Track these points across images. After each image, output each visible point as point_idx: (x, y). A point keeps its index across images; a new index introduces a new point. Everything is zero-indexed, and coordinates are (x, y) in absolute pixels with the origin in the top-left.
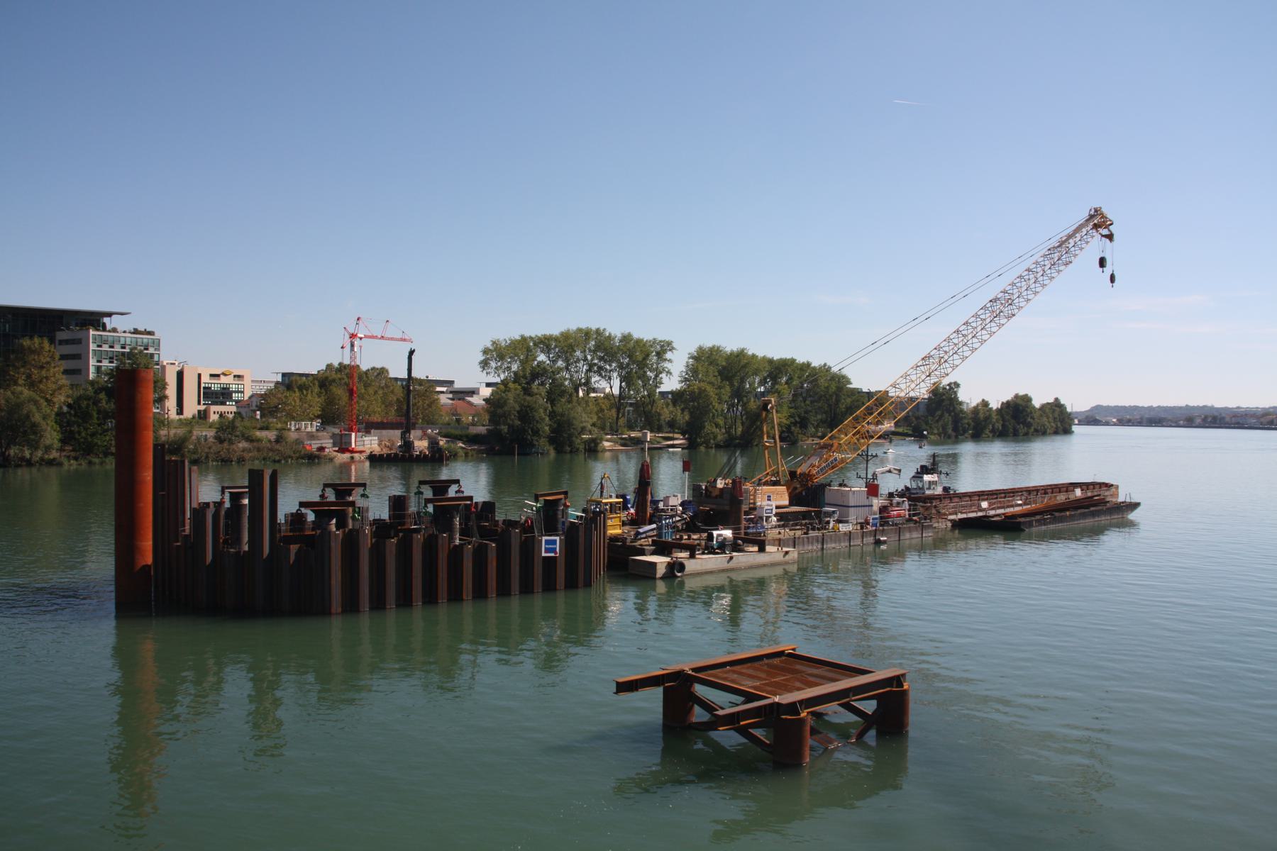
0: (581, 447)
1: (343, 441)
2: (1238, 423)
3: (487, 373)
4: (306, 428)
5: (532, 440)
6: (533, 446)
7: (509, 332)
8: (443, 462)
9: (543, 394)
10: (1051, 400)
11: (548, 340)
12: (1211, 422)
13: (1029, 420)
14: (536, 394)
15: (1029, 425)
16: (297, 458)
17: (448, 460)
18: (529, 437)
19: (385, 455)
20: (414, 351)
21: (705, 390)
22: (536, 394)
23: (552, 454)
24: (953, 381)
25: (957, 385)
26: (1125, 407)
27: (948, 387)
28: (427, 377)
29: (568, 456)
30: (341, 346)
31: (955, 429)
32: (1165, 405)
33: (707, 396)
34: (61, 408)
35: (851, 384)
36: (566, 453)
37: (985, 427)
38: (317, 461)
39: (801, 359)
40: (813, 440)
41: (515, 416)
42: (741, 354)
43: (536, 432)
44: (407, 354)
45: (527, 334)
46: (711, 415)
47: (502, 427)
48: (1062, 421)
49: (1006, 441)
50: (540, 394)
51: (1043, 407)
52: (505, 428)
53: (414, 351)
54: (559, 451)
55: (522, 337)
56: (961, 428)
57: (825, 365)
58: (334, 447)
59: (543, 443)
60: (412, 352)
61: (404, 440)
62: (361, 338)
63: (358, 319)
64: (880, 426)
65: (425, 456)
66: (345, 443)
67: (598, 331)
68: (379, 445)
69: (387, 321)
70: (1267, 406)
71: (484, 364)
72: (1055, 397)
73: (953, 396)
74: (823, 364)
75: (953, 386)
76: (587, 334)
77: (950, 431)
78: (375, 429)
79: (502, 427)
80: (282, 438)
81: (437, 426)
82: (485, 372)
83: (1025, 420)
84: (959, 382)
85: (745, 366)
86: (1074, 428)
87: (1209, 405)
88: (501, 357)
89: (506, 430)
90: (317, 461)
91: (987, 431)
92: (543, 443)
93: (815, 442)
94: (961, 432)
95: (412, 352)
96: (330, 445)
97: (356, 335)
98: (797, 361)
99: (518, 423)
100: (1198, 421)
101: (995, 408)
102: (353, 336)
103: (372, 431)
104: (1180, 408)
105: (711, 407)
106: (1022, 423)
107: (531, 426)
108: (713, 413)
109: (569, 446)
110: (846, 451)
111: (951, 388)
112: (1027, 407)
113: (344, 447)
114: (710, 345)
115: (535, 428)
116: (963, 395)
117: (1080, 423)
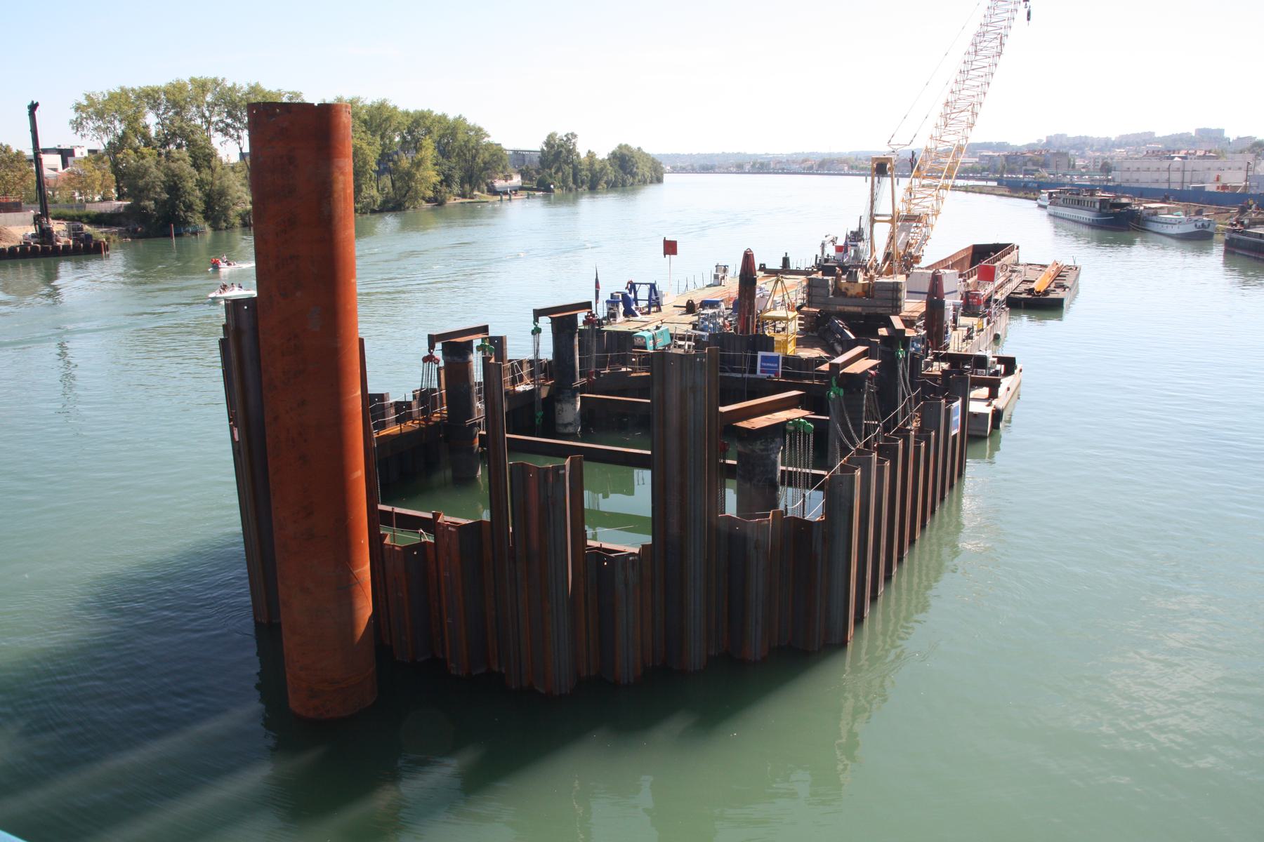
0: (238, 221)
2: (783, 169)
3: (82, 135)
5: (186, 217)
6: (189, 223)
7: (105, 84)
8: (101, 253)
9: (187, 158)
11: (157, 92)
12: (758, 168)
13: (635, 170)
14: (178, 160)
15: (633, 175)
17: (108, 250)
18: (182, 213)
19: (18, 249)
20: (37, 105)
21: (361, 148)
22: (178, 160)
23: (208, 230)
24: (570, 132)
25: (574, 136)
26: (668, 155)
27: (565, 139)
28: (59, 146)
29: (224, 234)
31: (575, 182)
32: (704, 153)
33: (363, 154)
35: (489, 136)
36: (221, 229)
37: (601, 179)
39: (438, 111)
40: (455, 200)
42: (381, 107)
43: (189, 207)
44: (27, 111)
45: (128, 86)
46: (368, 176)
47: (147, 203)
48: (655, 170)
49: (570, 206)
50: (184, 160)
52: (151, 204)
53: (37, 105)
54: (216, 228)
55: (122, 89)
56: (579, 181)
57: (460, 117)
59: (197, 220)
60: (33, 107)
61: (40, 227)
64: (509, 182)
65: (34, 248)
67: (215, 81)
70: (790, 153)
71: (78, 125)
72: (639, 146)
73: (571, 147)
74: (457, 116)
75: (570, 137)
76: (202, 86)
77: (571, 184)
79: (147, 203)
82: (79, 134)
83: (631, 171)
84: (576, 133)
85: (387, 119)
86: (666, 177)
87: (742, 151)
88: (100, 115)
89: (153, 206)
91: (602, 183)
92: (197, 220)
93: (457, 201)
94: (580, 185)
95: (33, 107)
98: (434, 114)
99: (165, 196)
100: (747, 167)
104: (718, 155)
105: (368, 167)
106: (629, 173)
107: (183, 199)
108: (370, 174)
109: (225, 221)
111: (569, 139)
112: (633, 157)
114: (1105, 137)
115: (187, 200)
116: (582, 150)
117: (675, 170)
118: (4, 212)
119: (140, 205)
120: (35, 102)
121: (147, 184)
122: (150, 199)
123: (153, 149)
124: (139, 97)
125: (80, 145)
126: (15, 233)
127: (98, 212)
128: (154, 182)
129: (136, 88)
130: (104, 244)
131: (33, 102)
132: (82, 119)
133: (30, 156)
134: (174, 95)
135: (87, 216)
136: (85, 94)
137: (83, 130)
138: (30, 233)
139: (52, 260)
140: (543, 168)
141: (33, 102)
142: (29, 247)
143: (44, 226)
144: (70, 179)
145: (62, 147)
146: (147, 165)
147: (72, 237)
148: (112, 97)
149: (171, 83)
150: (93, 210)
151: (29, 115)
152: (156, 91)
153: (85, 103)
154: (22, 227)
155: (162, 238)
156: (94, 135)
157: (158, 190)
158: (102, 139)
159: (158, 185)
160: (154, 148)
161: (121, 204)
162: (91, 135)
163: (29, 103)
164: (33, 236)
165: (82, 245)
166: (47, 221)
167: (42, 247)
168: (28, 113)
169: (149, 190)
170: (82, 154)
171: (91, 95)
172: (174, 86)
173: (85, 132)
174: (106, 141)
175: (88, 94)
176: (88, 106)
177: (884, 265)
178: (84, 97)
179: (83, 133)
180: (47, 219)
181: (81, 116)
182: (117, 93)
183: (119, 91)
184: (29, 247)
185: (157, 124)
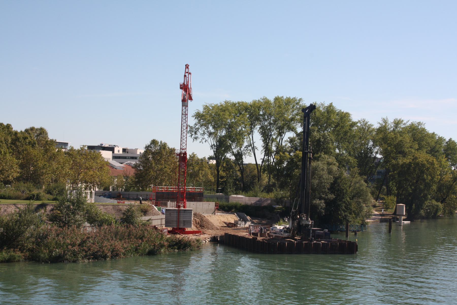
1: (181, 219)
28: (102, 144)
113: (181, 226)
162: (201, 139)
170: (119, 151)
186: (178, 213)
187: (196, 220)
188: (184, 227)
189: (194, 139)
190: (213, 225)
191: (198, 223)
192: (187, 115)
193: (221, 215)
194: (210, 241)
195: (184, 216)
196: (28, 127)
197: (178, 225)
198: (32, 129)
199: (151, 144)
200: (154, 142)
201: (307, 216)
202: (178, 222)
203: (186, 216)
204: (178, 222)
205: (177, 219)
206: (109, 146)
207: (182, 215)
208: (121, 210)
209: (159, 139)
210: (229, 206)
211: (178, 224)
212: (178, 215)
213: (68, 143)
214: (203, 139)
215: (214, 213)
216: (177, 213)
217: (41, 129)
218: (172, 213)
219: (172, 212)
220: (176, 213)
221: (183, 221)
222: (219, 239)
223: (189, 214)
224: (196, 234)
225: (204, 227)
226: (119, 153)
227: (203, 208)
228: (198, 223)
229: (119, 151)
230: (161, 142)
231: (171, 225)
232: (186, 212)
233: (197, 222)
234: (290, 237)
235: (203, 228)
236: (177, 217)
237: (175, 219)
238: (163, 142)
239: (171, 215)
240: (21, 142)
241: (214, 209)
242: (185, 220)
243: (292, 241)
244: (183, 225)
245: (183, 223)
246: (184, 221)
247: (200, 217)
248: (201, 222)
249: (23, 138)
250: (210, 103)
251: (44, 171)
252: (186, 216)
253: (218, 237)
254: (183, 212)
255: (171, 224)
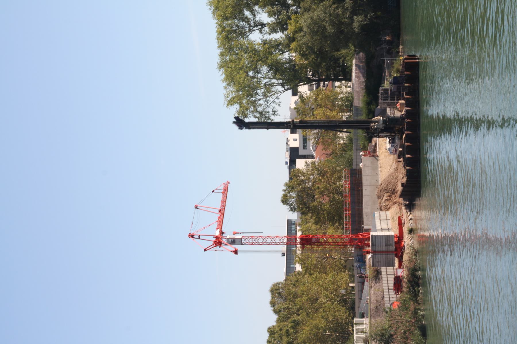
1: (384, 249)
4: (362, 332)
10: (267, 335)
16: (417, 301)
19: (408, 168)
28: (287, 163)
30: (233, 254)
34: (331, 34)
38: (419, 273)
41: (337, 8)
44: (245, 131)
47: (356, 25)
51: (296, 106)
52: (358, 20)
55: (221, 66)
58: (393, 265)
61: (382, 131)
62: (222, 233)
63: (192, 236)
65: (407, 139)
66: (387, 245)
68: (387, 209)
69: (196, 207)
78: (363, 224)
80: (383, 335)
81: (354, 157)
89: (360, 18)
90: (419, 273)
96: (390, 269)
97: (217, 237)
101: (296, 218)
102: (218, 243)
103: (365, 227)
110: (442, 227)
113: (393, 248)
118: (361, 186)
119: (358, 33)
120: (235, 120)
121: (332, 23)
122: (351, 19)
123: (291, 19)
124: (230, 49)
125: (285, 141)
126: (387, 176)
127: (364, 91)
128: (330, 15)
129: (219, 51)
130: (406, 59)
131: (234, 122)
132: (256, 111)
133: (298, 215)
134: (227, 7)
135: (368, 104)
136: (228, 105)
137: (268, 112)
138: (389, 146)
139: (423, 121)
140: (326, 228)
141: (234, 122)
142: (406, 73)
143: (381, 126)
144: (324, 143)
145: (288, 159)
146: (309, 21)
147: (396, 101)
148: (230, 79)
149: (213, 13)
150: (361, 98)
151: (250, 128)
152: (222, 29)
153: (237, 106)
154: (379, 169)
155: (402, 10)
156: (274, 102)
157: (340, 11)
158: (276, 92)
159: (334, 10)
160: (289, 18)
161: (356, 65)
162: (274, 105)
163: (236, 127)
164: (392, 141)
165: (406, 85)
166: (375, 122)
167: (407, 130)
168: (247, 130)
169: (341, 23)
170: (295, 140)
171: (229, 99)
172: (217, 8)
173: (270, 110)
174: (280, 88)
175: (226, 103)
176: (241, 104)
177: (431, 179)
178: (231, 107)
179: (271, 112)
180: (372, 122)
181: (252, 112)
182: (226, 71)
183: (223, 70)
184: (406, 73)
185: (261, 32)
186: (377, 253)
187: (385, 200)
188: (394, 244)
189: (276, 115)
190: (392, 174)
191: (389, 196)
192: (252, 244)
193: (380, 148)
194: (410, 211)
195: (379, 245)
196: (270, 309)
197: (392, 252)
198: (273, 304)
199: (288, 204)
200: (285, 201)
201: (372, 122)
202: (387, 252)
203: (379, 243)
204: (387, 252)
205: (384, 253)
206: (287, 151)
207: (379, 248)
208: (377, 307)
209: (280, 194)
210: (368, 112)
211: (390, 252)
212: (379, 253)
213: (288, 220)
214: (275, 102)
215: (377, 158)
216: (376, 255)
217: (272, 291)
218: (377, 260)
219: (375, 260)
220: (377, 256)
221: (386, 247)
222: (407, 203)
223: (377, 239)
224: (403, 223)
225: (394, 190)
226: (298, 140)
227: (370, 174)
228: (389, 196)
229: (295, 140)
230: (285, 191)
231: (391, 262)
232: (374, 244)
233: (388, 198)
234: (400, 136)
235: (395, 191)
236: (382, 253)
237: (384, 256)
238: (285, 188)
239: (379, 260)
240: (293, 339)
241: (371, 158)
242: (384, 245)
243: (405, 137)
244: (391, 247)
245: (389, 247)
246: (386, 246)
247: (382, 192)
248: (388, 192)
249: (287, 336)
250: (224, 99)
251: (331, 319)
252: (379, 243)
253: (405, 202)
254: (374, 247)
255: (390, 261)
